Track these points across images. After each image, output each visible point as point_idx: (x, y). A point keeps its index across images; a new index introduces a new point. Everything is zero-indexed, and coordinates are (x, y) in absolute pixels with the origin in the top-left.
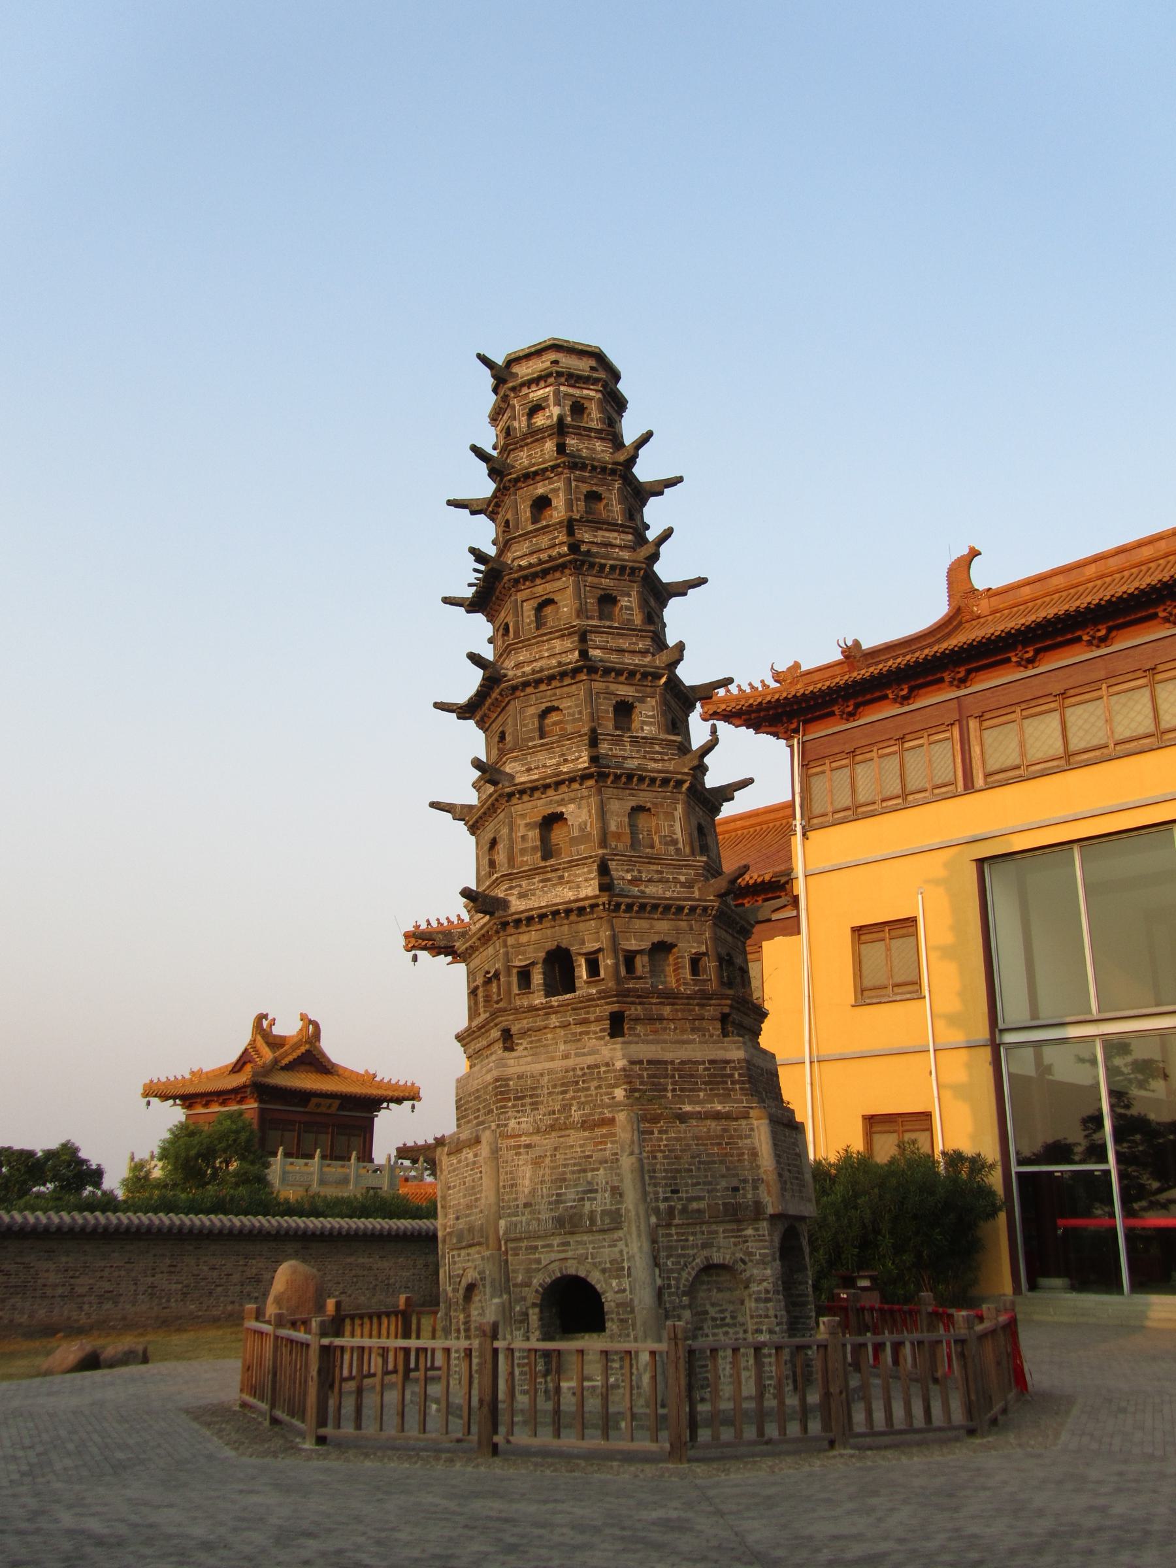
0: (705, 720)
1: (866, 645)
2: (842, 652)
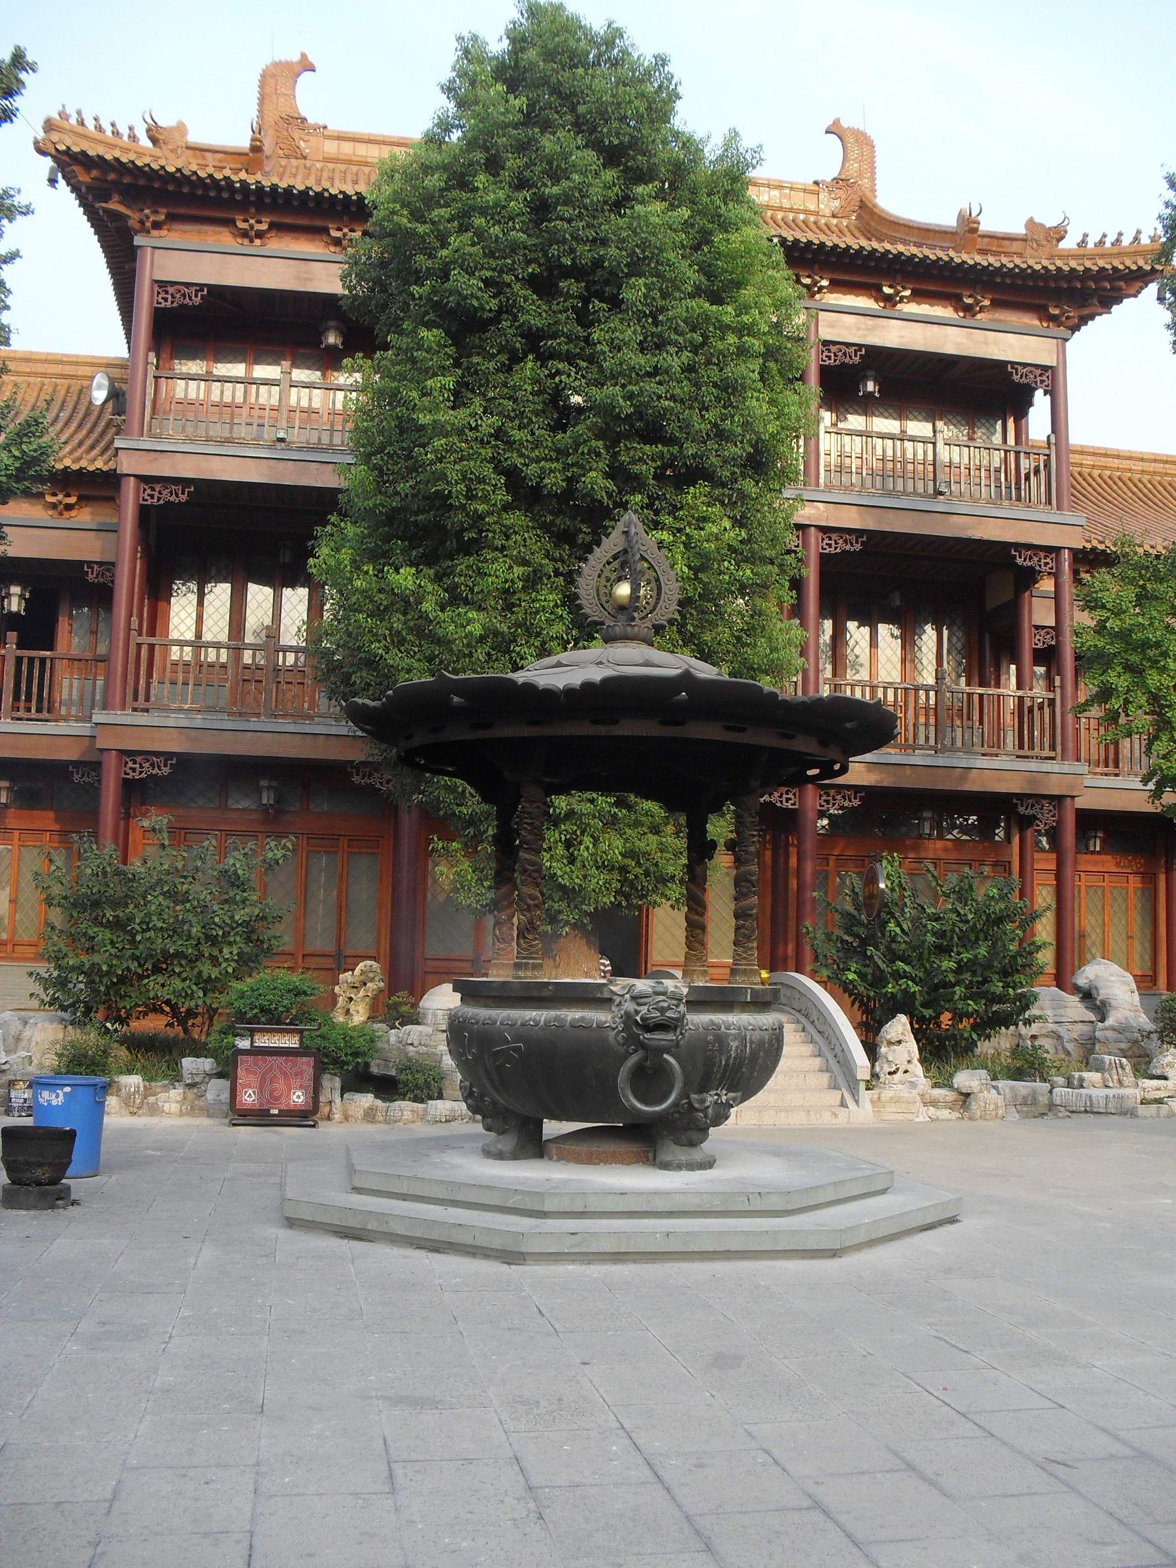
0: (41, 152)
1: (195, 136)
2: (253, 140)
